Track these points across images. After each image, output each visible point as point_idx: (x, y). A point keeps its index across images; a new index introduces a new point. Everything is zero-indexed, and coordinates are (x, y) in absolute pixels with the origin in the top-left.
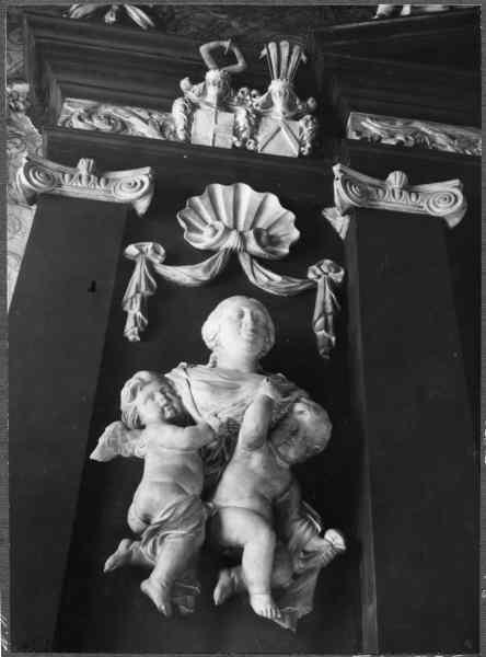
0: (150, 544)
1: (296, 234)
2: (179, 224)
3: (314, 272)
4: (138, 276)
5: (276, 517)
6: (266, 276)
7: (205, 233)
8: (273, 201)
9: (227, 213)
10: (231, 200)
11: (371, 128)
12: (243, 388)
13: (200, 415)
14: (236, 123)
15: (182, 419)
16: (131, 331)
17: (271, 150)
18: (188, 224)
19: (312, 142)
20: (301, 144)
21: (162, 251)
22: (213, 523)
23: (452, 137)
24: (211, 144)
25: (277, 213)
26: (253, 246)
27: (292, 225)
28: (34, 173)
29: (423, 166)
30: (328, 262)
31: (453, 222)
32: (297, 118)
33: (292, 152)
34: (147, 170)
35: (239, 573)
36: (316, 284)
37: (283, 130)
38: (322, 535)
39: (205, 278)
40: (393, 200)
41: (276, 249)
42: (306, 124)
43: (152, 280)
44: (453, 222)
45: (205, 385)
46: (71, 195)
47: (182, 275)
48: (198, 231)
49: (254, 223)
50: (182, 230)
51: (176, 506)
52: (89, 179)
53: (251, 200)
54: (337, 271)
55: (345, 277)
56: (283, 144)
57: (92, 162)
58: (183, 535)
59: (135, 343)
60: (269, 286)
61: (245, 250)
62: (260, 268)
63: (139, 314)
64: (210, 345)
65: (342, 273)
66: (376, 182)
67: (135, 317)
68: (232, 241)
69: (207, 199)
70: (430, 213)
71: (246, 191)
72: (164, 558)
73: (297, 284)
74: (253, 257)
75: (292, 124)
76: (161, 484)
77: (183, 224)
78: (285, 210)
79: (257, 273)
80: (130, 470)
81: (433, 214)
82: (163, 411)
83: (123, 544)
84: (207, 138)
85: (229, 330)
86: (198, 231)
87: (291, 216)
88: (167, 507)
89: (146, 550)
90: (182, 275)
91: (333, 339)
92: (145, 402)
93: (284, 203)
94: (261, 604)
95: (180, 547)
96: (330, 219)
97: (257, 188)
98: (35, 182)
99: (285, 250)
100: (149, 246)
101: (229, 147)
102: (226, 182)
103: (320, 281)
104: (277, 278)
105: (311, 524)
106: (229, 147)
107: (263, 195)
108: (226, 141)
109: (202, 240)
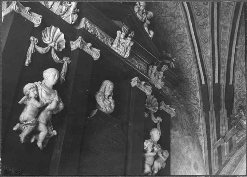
0: (24, 126)
1: (64, 47)
2: (42, 33)
3: (65, 59)
4: (32, 45)
5: (47, 125)
6: (56, 57)
7: (47, 39)
8: (63, 36)
9: (53, 34)
10: (54, 31)
11: (88, 25)
12: (52, 95)
13: (42, 99)
14: (62, 9)
15: (38, 99)
16: (27, 63)
17: (66, 20)
18: (45, 36)
19: (75, 22)
20: (73, 21)
21: (38, 41)
22: (37, 124)
23: (101, 34)
24: (55, 13)
25: (62, 39)
26: (56, 48)
27: (64, 44)
28: (17, 6)
29: (97, 43)
30: (69, 58)
31: (94, 60)
32: (74, 14)
33: (70, 21)
34: (72, 50)
35: (37, 136)
36: (64, 62)
37: (71, 16)
38: (52, 130)
39: (44, 53)
40: (87, 49)
41: (59, 49)
42: (76, 17)
43: (34, 50)
44: (94, 60)
45: (45, 92)
46: (22, 15)
47: (40, 50)
48: (46, 38)
49: (59, 42)
50: (42, 36)
51: (33, 121)
52: (28, 13)
53: (58, 33)
54: (69, 61)
55: (70, 63)
56: (69, 19)
57: (30, 9)
58: (32, 128)
59: (27, 66)
60: (56, 60)
61: (54, 48)
62: (56, 55)
63: (30, 59)
64: (44, 77)
65: (70, 62)
66: (85, 43)
67: (29, 60)
68: (52, 44)
69: (50, 29)
70: (92, 55)
71: (58, 30)
72: (26, 131)
73: (61, 62)
74: (55, 50)
75: (73, 15)
76: (32, 114)
77: (43, 34)
78: (64, 39)
79: (55, 56)
80: (24, 106)
81: (92, 56)
82: (35, 96)
83: (18, 125)
84: (55, 10)
85: (50, 76)
86: (46, 38)
87: (65, 41)
88: (31, 121)
89: (23, 128)
90: (40, 50)
91: (64, 80)
92: (32, 92)
93: (65, 37)
94: (39, 144)
95: (31, 130)
96: (71, 44)
97: (61, 31)
98: (17, 9)
99: (61, 50)
100: (36, 39)
101: (58, 15)
102: (55, 27)
103: (65, 62)
104: (58, 59)
105: (51, 128)
106: (58, 15)
107: (61, 33)
108: (58, 13)
109: (46, 40)
